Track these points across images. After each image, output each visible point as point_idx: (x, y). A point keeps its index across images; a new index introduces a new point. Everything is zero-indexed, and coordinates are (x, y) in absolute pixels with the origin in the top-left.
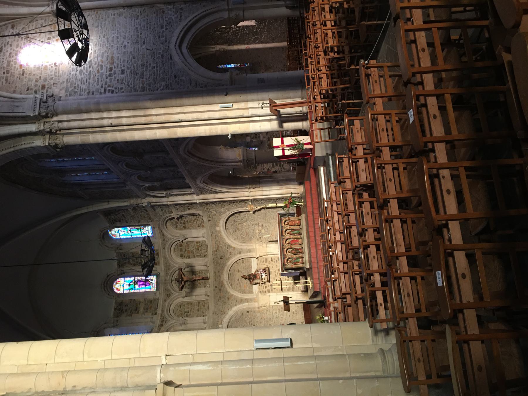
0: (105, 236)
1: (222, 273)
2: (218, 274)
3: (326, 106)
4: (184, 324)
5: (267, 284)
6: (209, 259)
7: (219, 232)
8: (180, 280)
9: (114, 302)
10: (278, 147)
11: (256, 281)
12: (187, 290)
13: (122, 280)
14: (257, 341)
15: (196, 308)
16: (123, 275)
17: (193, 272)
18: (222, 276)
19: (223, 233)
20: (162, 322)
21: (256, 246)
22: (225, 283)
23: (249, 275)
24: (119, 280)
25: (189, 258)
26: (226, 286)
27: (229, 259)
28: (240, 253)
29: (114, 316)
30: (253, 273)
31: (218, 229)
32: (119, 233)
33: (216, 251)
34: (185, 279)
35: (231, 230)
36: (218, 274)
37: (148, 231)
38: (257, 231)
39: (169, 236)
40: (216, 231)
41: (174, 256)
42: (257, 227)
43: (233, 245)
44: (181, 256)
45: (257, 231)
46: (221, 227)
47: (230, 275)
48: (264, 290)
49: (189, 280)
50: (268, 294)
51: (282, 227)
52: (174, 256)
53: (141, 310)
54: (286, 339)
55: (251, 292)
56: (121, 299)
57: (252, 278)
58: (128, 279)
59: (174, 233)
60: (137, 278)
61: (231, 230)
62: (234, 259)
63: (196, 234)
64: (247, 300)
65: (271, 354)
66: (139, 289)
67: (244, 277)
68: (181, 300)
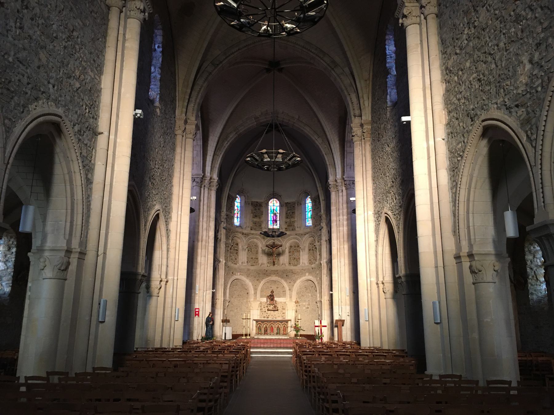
0: (307, 194)
1: (276, 276)
2: (276, 272)
3: (512, 392)
4: (243, 249)
5: (267, 309)
6: (288, 267)
7: (305, 275)
8: (273, 246)
9: (262, 201)
10: (321, 323)
11: (269, 300)
12: (266, 250)
13: (278, 204)
14: (178, 309)
15: (254, 257)
16: (281, 206)
17: (279, 254)
18: (274, 276)
19: (304, 278)
20: (245, 234)
21: (534, 248)
22: (269, 278)
23: (273, 296)
24: (278, 202)
25: (289, 252)
26: (267, 279)
27: (286, 281)
28: (290, 290)
29: (252, 202)
30: (275, 299)
31: (307, 274)
32: (309, 203)
33: (292, 272)
34: (274, 249)
35: (306, 284)
36: (276, 273)
37: (309, 223)
38: (304, 304)
39: (304, 239)
40: (306, 273)
41: (291, 241)
42: (307, 303)
43: (295, 285)
44: (291, 247)
45: (304, 304)
46: (308, 277)
47: (275, 282)
48: (262, 306)
49: (273, 253)
50: (259, 309)
51: (282, 322)
52: (291, 241)
53: (255, 220)
54: (178, 318)
55: (262, 296)
56: (264, 205)
57: (271, 297)
58: (278, 208)
59: (305, 242)
60: (278, 215)
61: (306, 284)
62: (285, 284)
63: (304, 258)
64: (255, 293)
65: (173, 313)
66: (271, 216)
67: (272, 292)
68: (260, 245)
